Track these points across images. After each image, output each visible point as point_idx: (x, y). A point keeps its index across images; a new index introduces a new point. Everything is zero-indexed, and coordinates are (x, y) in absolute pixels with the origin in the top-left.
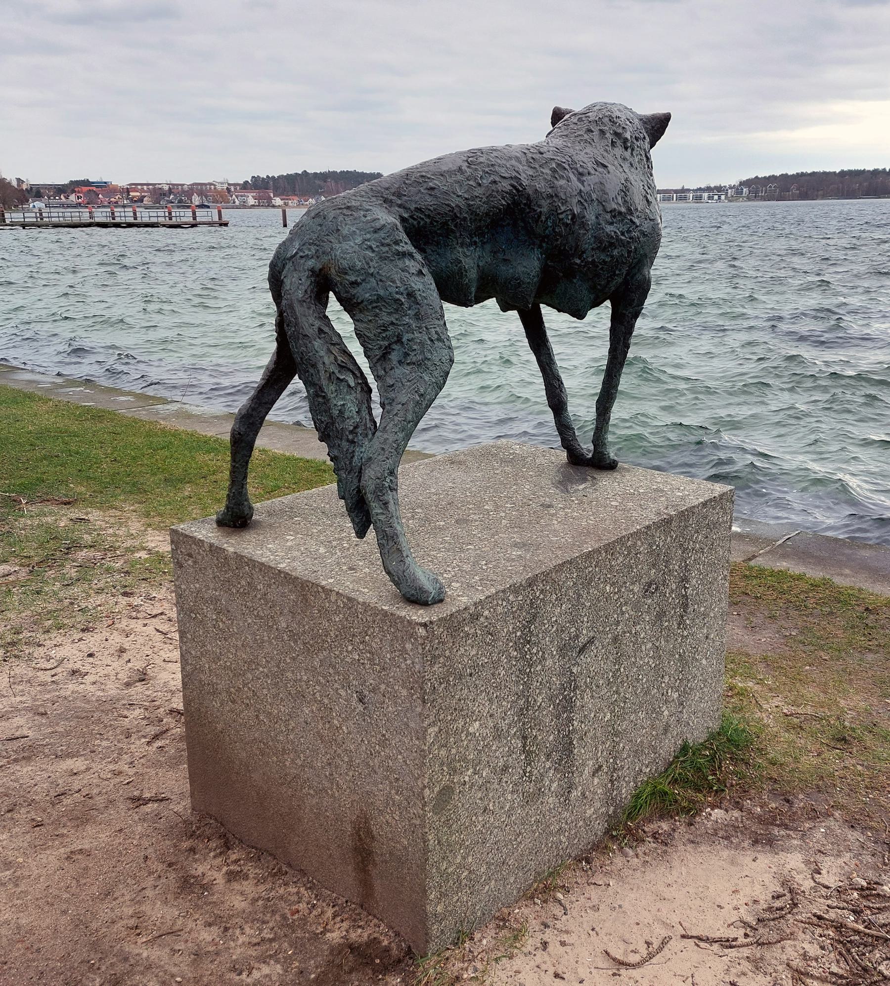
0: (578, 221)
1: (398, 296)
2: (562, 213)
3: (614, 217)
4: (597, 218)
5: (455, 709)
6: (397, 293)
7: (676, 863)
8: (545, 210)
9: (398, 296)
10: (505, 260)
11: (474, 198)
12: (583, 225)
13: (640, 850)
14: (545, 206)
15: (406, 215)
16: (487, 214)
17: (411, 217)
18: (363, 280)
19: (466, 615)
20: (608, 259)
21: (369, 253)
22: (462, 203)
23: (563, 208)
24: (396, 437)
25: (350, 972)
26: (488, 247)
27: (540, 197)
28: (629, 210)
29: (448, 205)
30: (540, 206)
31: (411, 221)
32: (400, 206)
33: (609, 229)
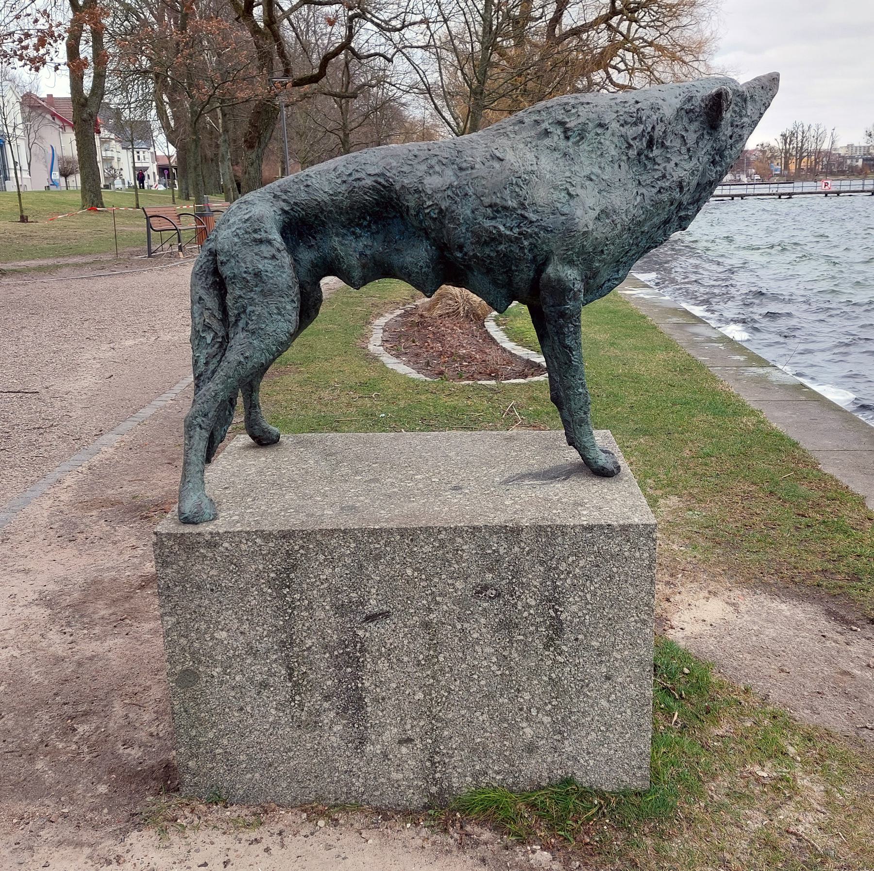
0: (448, 215)
1: (245, 275)
2: (427, 208)
3: (498, 211)
4: (473, 212)
5: (195, 612)
6: (245, 272)
7: (439, 864)
8: (412, 204)
9: (245, 275)
10: (397, 250)
11: (336, 194)
12: (453, 219)
13: (439, 838)
14: (411, 202)
15: (287, 208)
16: (351, 208)
17: (292, 209)
18: (228, 260)
19: (200, 539)
20: (493, 254)
21: (236, 240)
22: (326, 198)
23: (429, 203)
24: (216, 388)
25: (154, 779)
26: (380, 237)
27: (407, 192)
28: (522, 206)
29: (316, 200)
30: (407, 201)
31: (292, 213)
32: (284, 201)
33: (488, 224)
